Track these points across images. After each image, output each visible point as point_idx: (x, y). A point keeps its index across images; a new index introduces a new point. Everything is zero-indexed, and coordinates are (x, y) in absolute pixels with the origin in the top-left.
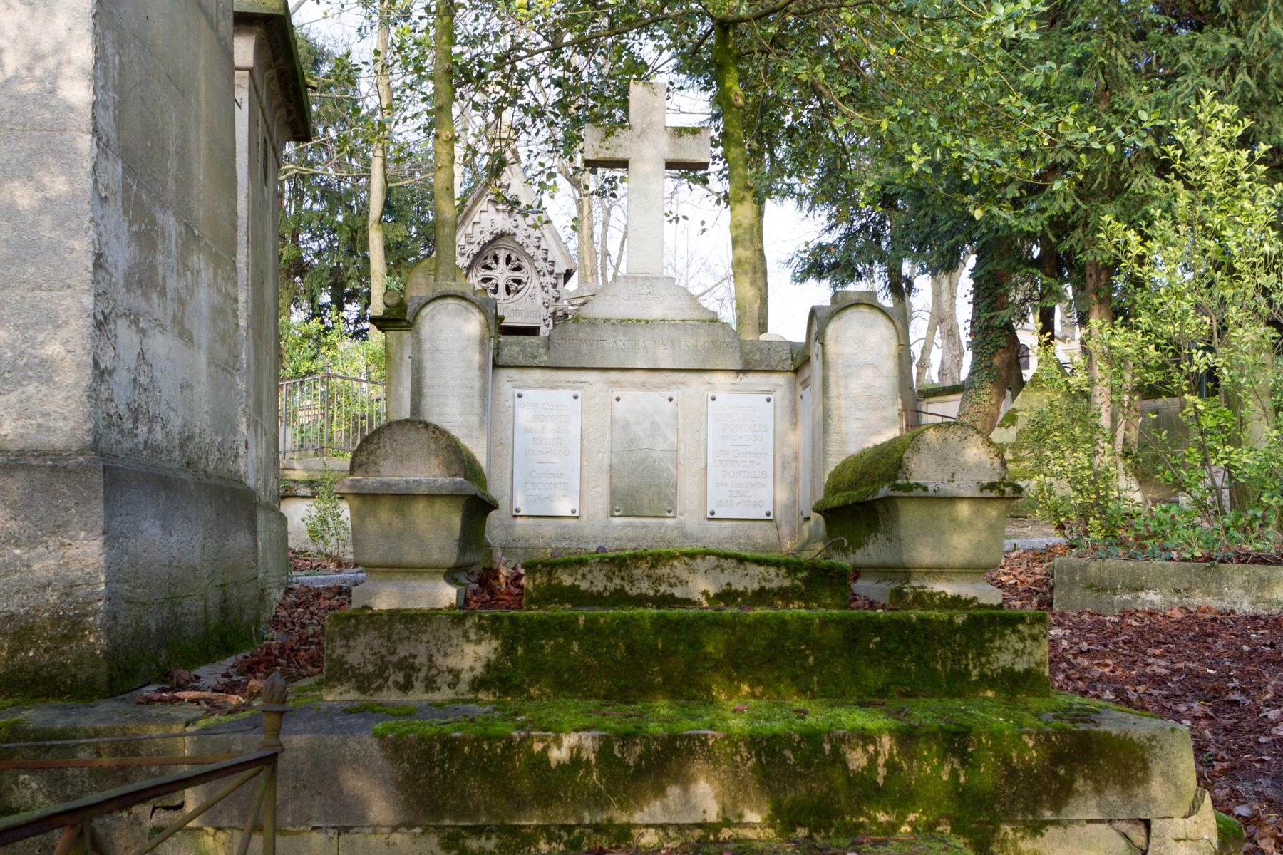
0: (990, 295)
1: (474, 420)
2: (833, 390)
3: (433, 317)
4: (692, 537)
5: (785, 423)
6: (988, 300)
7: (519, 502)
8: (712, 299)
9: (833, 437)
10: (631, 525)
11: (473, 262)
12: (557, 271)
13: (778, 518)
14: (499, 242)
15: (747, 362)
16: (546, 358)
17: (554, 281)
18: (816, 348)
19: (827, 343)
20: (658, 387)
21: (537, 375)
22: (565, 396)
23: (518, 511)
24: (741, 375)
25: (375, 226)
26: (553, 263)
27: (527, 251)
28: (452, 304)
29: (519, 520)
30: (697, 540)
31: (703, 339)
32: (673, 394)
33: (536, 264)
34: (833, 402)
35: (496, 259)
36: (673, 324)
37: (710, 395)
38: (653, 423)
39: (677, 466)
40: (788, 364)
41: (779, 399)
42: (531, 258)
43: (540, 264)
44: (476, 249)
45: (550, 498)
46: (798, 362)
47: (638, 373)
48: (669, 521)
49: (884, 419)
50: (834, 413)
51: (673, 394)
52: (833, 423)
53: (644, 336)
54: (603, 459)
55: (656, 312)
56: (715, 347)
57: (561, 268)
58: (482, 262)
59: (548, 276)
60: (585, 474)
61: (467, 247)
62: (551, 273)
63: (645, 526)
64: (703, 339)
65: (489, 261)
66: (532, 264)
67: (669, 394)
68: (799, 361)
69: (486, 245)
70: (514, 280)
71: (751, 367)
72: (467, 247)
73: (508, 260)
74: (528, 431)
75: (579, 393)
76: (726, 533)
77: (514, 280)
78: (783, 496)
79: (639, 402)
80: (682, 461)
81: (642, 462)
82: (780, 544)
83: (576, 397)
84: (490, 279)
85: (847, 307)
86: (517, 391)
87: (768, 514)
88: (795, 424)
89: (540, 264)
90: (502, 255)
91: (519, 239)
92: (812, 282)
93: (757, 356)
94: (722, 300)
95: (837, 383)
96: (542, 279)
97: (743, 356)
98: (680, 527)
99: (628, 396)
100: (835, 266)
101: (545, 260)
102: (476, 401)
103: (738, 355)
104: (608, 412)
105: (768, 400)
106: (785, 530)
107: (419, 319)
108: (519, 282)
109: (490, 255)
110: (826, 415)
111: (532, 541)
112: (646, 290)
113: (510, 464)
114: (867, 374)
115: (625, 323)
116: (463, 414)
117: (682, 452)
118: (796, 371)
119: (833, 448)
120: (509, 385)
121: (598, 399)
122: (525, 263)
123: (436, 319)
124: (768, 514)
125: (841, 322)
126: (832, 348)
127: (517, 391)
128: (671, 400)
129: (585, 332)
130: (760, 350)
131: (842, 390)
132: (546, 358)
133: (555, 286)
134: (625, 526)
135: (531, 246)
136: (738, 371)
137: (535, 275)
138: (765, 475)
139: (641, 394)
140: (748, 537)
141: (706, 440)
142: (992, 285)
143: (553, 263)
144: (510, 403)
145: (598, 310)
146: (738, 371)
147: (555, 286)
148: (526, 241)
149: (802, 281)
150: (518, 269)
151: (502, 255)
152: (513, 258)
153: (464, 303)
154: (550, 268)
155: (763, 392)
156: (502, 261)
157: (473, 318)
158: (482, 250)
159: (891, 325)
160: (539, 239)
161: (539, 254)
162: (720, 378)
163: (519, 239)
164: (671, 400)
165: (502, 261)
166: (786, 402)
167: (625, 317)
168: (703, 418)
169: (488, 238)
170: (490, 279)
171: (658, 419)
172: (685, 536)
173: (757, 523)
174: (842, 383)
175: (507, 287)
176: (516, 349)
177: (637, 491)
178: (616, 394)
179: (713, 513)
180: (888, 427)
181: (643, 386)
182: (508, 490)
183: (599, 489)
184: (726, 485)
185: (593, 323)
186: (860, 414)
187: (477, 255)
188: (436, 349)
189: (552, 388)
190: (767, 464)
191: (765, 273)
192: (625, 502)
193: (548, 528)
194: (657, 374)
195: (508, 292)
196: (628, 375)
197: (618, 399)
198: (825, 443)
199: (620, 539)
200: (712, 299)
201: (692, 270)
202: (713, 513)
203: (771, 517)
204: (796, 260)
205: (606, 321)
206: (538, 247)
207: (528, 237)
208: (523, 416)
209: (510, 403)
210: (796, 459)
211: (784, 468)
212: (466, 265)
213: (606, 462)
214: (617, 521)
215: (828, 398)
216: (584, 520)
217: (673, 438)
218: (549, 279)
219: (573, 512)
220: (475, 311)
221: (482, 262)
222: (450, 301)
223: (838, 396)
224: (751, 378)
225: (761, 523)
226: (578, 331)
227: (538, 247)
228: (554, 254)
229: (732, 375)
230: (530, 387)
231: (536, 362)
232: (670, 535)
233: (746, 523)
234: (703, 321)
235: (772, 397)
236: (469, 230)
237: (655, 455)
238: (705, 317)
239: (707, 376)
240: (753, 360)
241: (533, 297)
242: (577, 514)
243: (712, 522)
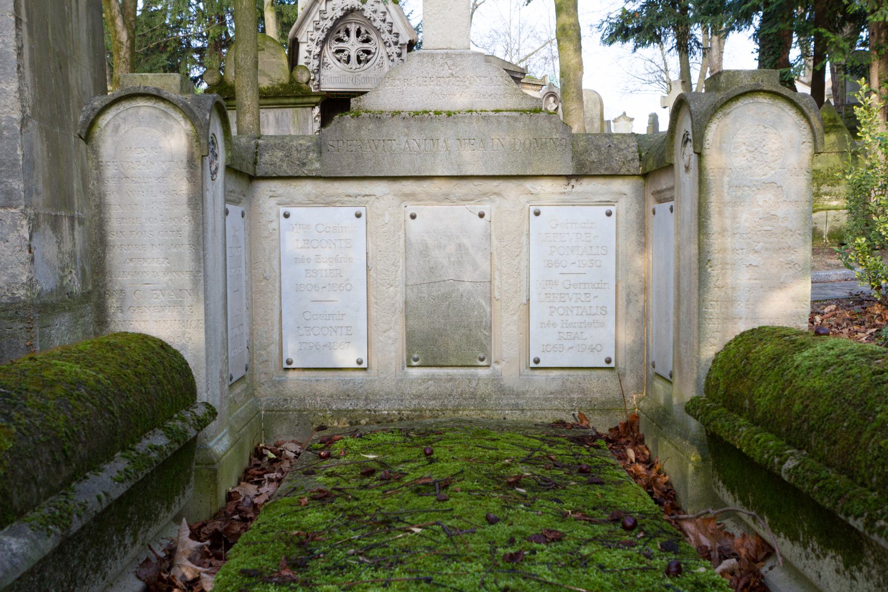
0: (774, 53)
1: (185, 279)
2: (714, 223)
3: (116, 129)
4: (512, 392)
5: (630, 244)
6: (772, 58)
7: (291, 350)
8: (538, 58)
9: (714, 294)
10: (433, 378)
11: (327, 36)
12: (401, 42)
13: (621, 365)
14: (350, 17)
15: (580, 164)
16: (317, 165)
17: (398, 51)
18: (684, 156)
19: (706, 152)
20: (464, 200)
21: (308, 188)
22: (345, 214)
23: (289, 362)
24: (573, 182)
25: (269, 7)
26: (397, 35)
27: (375, 24)
28: (144, 107)
29: (291, 375)
30: (518, 395)
31: (522, 134)
32: (485, 207)
33: (383, 36)
34: (716, 242)
35: (348, 32)
36: (483, 116)
37: (532, 209)
38: (460, 246)
39: (490, 300)
40: (636, 166)
41: (622, 212)
42: (378, 31)
43: (386, 36)
44: (330, 24)
45: (329, 346)
46: (652, 162)
47: (437, 182)
48: (482, 372)
49: (791, 264)
50: (716, 257)
51: (485, 207)
52: (714, 272)
53: (445, 133)
54: (396, 294)
55: (460, 100)
56: (539, 145)
57: (405, 39)
58: (335, 35)
59: (393, 47)
60: (373, 313)
61: (321, 23)
62: (396, 43)
63: (451, 379)
64: (522, 134)
65: (341, 35)
66: (379, 36)
67: (479, 208)
68: (651, 164)
69: (338, 21)
70: (364, 51)
71: (585, 171)
72: (321, 23)
73: (358, 33)
74: (297, 260)
75: (362, 210)
76: (554, 386)
77: (364, 51)
78: (627, 337)
79: (441, 221)
80: (496, 294)
81: (445, 297)
82: (624, 400)
83: (358, 216)
84: (343, 51)
85: (737, 97)
86: (283, 210)
87: (608, 361)
88: (643, 245)
89: (386, 36)
90: (353, 28)
91: (367, 14)
92: (618, 44)
93: (594, 157)
94: (546, 59)
95: (720, 213)
96: (388, 49)
97: (577, 157)
98: (496, 379)
99: (425, 211)
100: (639, 30)
101: (390, 32)
102: (187, 251)
103: (568, 156)
104: (402, 233)
105: (609, 214)
106: (630, 381)
107: (97, 131)
108: (368, 52)
109: (342, 28)
110: (703, 259)
111: (308, 401)
112: (447, 72)
113: (277, 302)
114: (765, 200)
115: (420, 116)
116: (168, 271)
117: (496, 283)
118: (645, 176)
119: (714, 310)
120: (273, 202)
121: (387, 218)
122: (373, 36)
123: (122, 131)
124: (608, 361)
125: (728, 120)
126: (713, 159)
127: (283, 210)
128: (481, 215)
129: (368, 130)
130: (598, 148)
131: (728, 222)
132: (317, 165)
133: (399, 55)
134: (425, 380)
135: (378, 20)
136: (569, 177)
137: (382, 45)
138: (604, 311)
139: (443, 209)
140: (583, 391)
141: (528, 267)
142: (776, 45)
143: (397, 35)
144: (274, 225)
145: (384, 98)
146: (569, 177)
147: (399, 55)
148: (373, 15)
149: (611, 43)
150: (367, 41)
151: (353, 28)
152: (363, 31)
153: (162, 105)
154: (395, 40)
155: (601, 203)
156: (353, 34)
157: (176, 128)
158: (335, 24)
159: (803, 123)
160: (384, 13)
161: (385, 27)
162: (546, 187)
163: (367, 14)
164: (481, 215)
165: (353, 34)
166: (632, 216)
167: (420, 107)
168: (524, 238)
169: (340, 14)
170: (343, 51)
171: (466, 241)
172: (502, 390)
173: (594, 372)
174: (728, 212)
175: (358, 57)
176: (280, 154)
177: (442, 333)
178: (412, 209)
179: (537, 361)
180: (795, 277)
181: (446, 198)
182: (276, 336)
183: (392, 333)
184: (554, 325)
185: (378, 117)
186: (753, 258)
187: (331, 30)
188: (123, 177)
189: (328, 204)
190: (607, 298)
191: (579, 39)
192: (424, 348)
193: (327, 384)
194: (463, 183)
195: (359, 62)
196: (426, 185)
197: (413, 217)
198: (701, 301)
199: (419, 396)
200: (538, 58)
201: (523, 36)
202: (537, 361)
203: (612, 365)
204: (605, 25)
205: (396, 114)
206: (384, 21)
207: (375, 12)
208: (292, 241)
209: (274, 225)
210: (645, 290)
211: (629, 302)
212: (321, 39)
213: (400, 299)
214: (415, 372)
215: (707, 235)
216: (373, 372)
217: (485, 266)
218: (395, 49)
219: (360, 362)
220: (179, 116)
221: (335, 35)
222: (141, 103)
223: (723, 231)
224: (586, 186)
225: (600, 372)
226: (358, 128)
227: (384, 21)
228: (398, 27)
229: (563, 182)
230: (300, 204)
231: (305, 171)
232: (482, 389)
233: (580, 373)
234: (524, 111)
235: (613, 209)
236: (323, 8)
237: (462, 288)
238: (525, 105)
239: (529, 185)
240: (591, 158)
241: (381, 66)
242: (364, 365)
243: (537, 372)
